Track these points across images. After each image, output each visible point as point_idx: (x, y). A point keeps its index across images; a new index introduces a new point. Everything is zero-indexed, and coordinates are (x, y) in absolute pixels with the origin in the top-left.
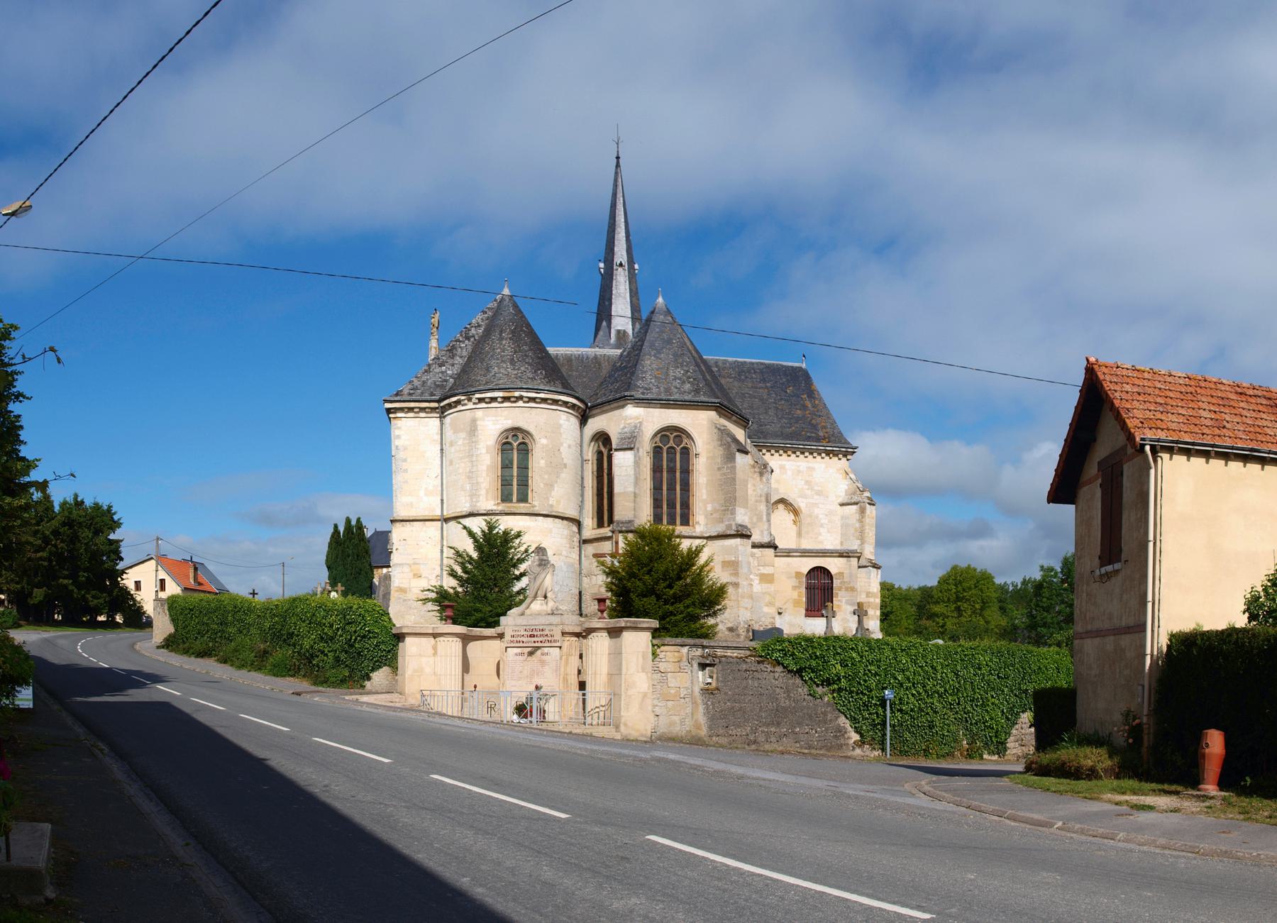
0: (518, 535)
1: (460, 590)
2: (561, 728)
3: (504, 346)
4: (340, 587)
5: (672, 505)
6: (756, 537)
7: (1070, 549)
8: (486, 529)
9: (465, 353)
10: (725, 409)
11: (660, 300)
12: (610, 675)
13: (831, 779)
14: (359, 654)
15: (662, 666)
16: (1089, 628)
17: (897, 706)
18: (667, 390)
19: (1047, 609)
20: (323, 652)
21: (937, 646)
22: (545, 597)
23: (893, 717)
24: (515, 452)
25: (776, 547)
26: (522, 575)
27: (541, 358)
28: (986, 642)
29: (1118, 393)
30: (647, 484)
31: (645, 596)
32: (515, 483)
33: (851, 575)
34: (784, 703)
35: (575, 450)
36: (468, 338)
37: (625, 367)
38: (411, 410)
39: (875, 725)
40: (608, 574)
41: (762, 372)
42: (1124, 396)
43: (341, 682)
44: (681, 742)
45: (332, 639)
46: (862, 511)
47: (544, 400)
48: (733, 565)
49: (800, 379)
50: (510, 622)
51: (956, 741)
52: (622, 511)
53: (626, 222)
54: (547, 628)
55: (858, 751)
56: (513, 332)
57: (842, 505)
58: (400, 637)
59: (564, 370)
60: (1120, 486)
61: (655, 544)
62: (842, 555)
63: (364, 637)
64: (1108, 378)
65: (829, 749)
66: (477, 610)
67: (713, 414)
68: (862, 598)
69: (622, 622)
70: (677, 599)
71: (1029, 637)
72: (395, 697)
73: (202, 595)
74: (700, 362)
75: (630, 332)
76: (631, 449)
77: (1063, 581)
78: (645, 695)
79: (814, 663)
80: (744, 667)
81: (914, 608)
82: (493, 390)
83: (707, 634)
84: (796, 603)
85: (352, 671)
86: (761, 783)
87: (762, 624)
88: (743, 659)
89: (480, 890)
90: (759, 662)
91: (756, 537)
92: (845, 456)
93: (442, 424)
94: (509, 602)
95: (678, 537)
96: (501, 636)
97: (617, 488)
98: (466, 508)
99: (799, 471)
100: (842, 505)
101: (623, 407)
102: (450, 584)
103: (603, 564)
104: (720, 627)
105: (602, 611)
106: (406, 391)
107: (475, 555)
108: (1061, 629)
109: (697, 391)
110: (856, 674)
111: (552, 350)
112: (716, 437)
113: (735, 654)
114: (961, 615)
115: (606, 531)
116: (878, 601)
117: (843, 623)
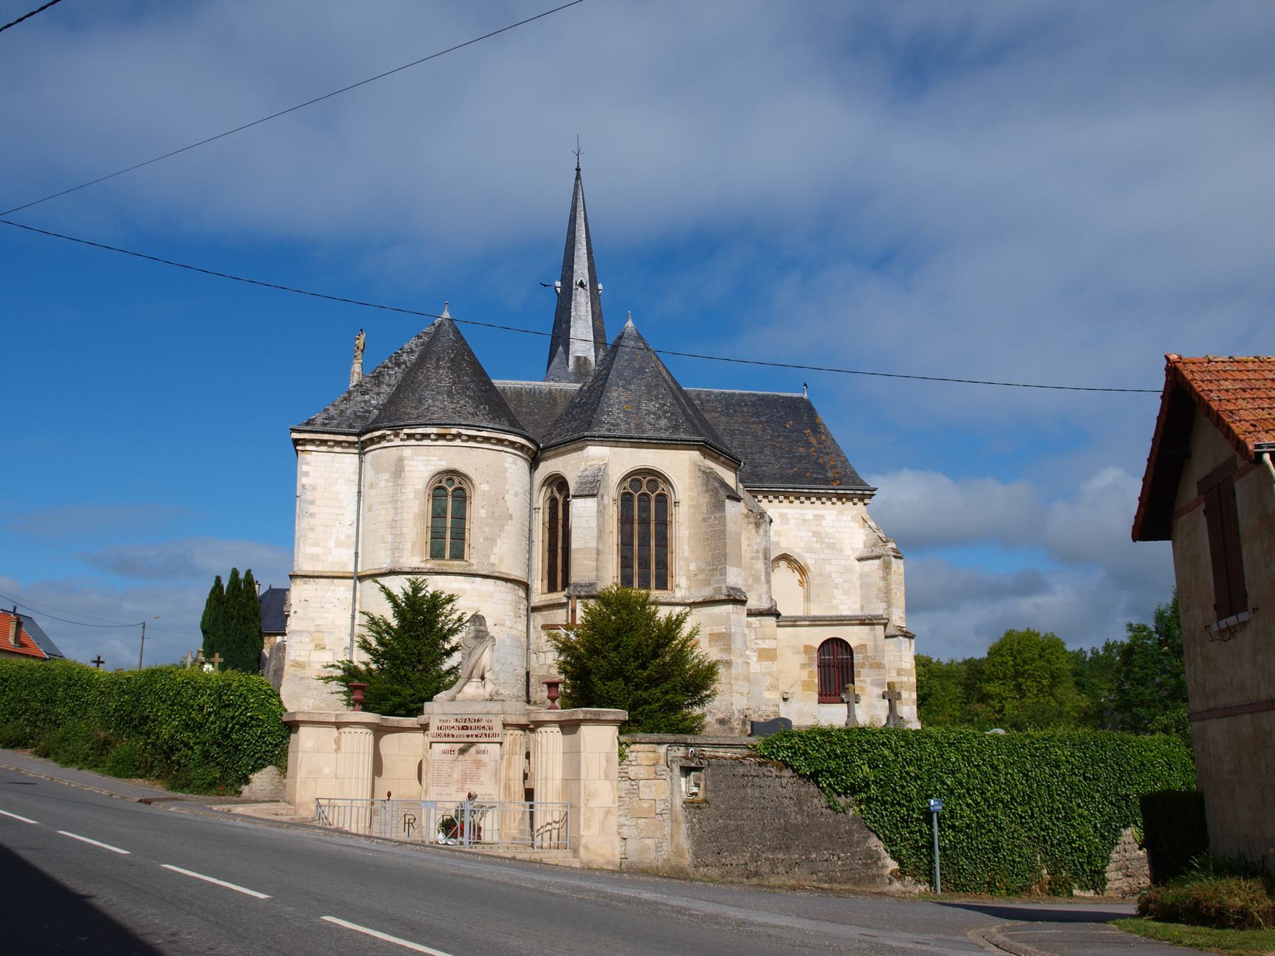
0: (450, 599)
1: (374, 666)
2: (501, 852)
3: (441, 376)
4: (218, 658)
5: (644, 564)
6: (753, 603)
7: (1167, 600)
8: (410, 591)
9: (393, 382)
10: (710, 448)
11: (630, 324)
12: (565, 780)
14: (236, 747)
15: (632, 771)
16: (1212, 704)
18: (639, 427)
19: (1142, 682)
20: (186, 745)
21: (996, 738)
22: (483, 678)
25: (778, 615)
26: (454, 649)
27: (486, 391)
28: (1060, 731)
29: (1214, 393)
30: (613, 539)
31: (610, 679)
32: (448, 535)
33: (876, 648)
36: (398, 365)
38: (324, 442)
39: (918, 849)
40: (561, 651)
41: (754, 405)
42: (1223, 396)
43: (210, 787)
44: (657, 875)
45: (200, 726)
46: (887, 567)
47: (487, 440)
48: (723, 639)
50: (437, 709)
51: (1032, 869)
52: (581, 571)
53: (588, 237)
54: (484, 718)
55: (897, 885)
56: (452, 360)
57: (860, 559)
58: (292, 727)
59: (512, 407)
60: (1233, 509)
61: (624, 612)
62: (862, 622)
63: (245, 724)
64: (1197, 376)
65: (857, 882)
66: (394, 693)
68: (892, 677)
69: (580, 713)
70: (653, 682)
71: (1122, 721)
73: (24, 660)
74: (678, 394)
75: (593, 360)
76: (593, 496)
77: (1161, 643)
78: (608, 812)
79: (833, 764)
80: (741, 770)
81: (960, 689)
82: (426, 425)
85: (225, 771)
86: (771, 931)
87: (763, 713)
90: (760, 764)
92: (861, 500)
93: (361, 462)
94: (437, 683)
95: (653, 603)
96: (424, 728)
97: (575, 543)
98: (385, 565)
99: (805, 521)
100: (860, 559)
101: (582, 449)
102: (361, 658)
103: (555, 638)
104: (708, 719)
106: (319, 421)
107: (394, 623)
108: (1166, 708)
109: (676, 428)
110: (890, 778)
111: (497, 383)
112: (700, 481)
113: (729, 753)
114: (1024, 696)
115: (559, 596)
116: (913, 680)
117: (870, 710)
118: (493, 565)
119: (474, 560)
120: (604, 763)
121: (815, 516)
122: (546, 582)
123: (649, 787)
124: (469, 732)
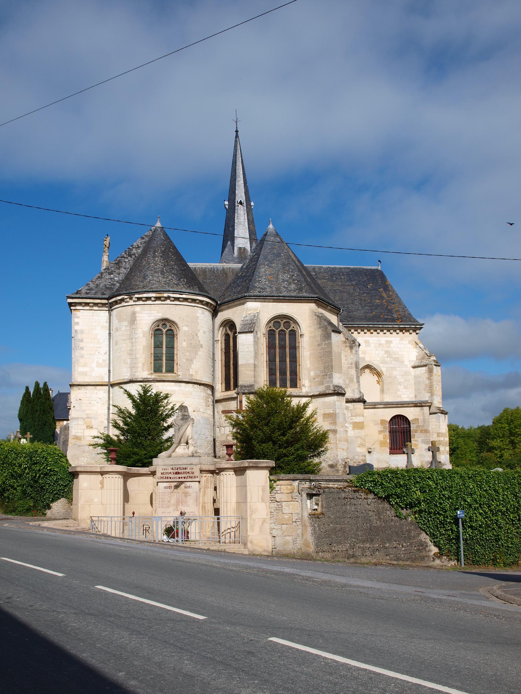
0: (166, 397)
1: (122, 438)
2: (201, 546)
3: (157, 262)
4: (29, 435)
5: (283, 373)
6: (349, 395)
8: (142, 392)
9: (128, 266)
11: (271, 226)
12: (238, 503)
13: (420, 587)
14: (42, 488)
15: (278, 497)
17: (468, 523)
18: (278, 289)
20: (13, 487)
21: (498, 473)
22: (187, 443)
23: (465, 533)
24: (164, 336)
25: (364, 402)
26: (169, 427)
27: (184, 270)
30: (264, 358)
31: (264, 442)
33: (424, 421)
34: (377, 523)
35: (209, 335)
36: (130, 256)
37: (245, 276)
38: (87, 304)
39: (450, 540)
40: (234, 426)
41: (348, 274)
43: (27, 511)
44: (294, 558)
45: (20, 476)
46: (431, 371)
47: (186, 300)
48: (332, 417)
49: (377, 278)
50: (160, 462)
54: (189, 467)
55: (438, 562)
56: (163, 252)
57: (414, 367)
58: (75, 475)
59: (200, 279)
62: (416, 405)
65: (414, 560)
66: (135, 454)
67: (313, 306)
68: (434, 438)
69: (246, 463)
70: (289, 444)
72: (70, 522)
74: (302, 269)
75: (249, 249)
76: (251, 332)
78: (264, 521)
79: (398, 491)
80: (343, 495)
82: (148, 292)
83: (313, 470)
84: (382, 444)
86: (361, 590)
87: (356, 460)
88: (342, 490)
89: (133, 683)
91: (349, 395)
93: (110, 315)
96: (153, 473)
97: (241, 361)
98: (127, 377)
99: (380, 344)
100: (414, 367)
102: (114, 433)
103: (230, 418)
104: (323, 464)
105: (229, 455)
106: (84, 291)
107: (133, 412)
109: (300, 290)
111: (191, 265)
112: (316, 322)
113: (336, 485)
115: (232, 393)
116: (447, 439)
117: (420, 458)
118: (192, 375)
119: (180, 372)
120: (261, 493)
121: (386, 341)
122: (224, 385)
123: (288, 506)
124: (180, 476)
